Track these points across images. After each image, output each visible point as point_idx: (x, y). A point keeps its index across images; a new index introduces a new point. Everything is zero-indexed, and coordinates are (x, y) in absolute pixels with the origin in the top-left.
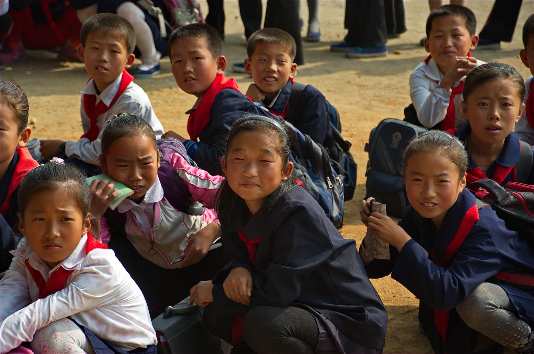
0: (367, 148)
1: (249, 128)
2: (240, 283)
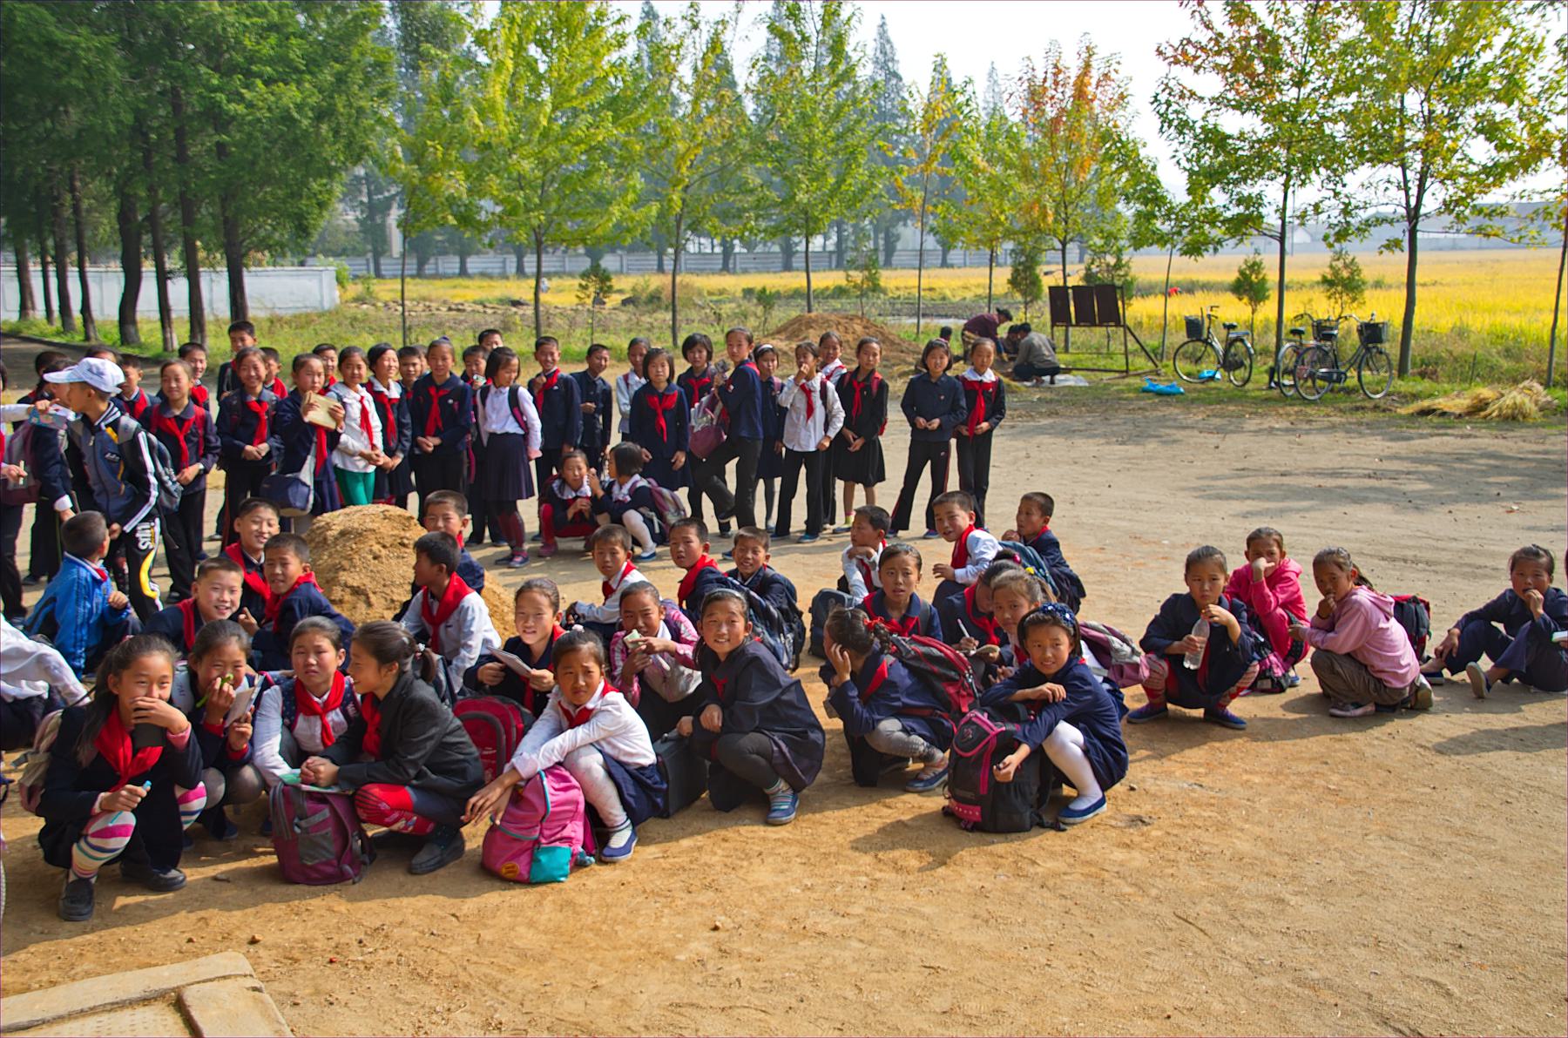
0: (810, 610)
1: (718, 599)
2: (713, 716)
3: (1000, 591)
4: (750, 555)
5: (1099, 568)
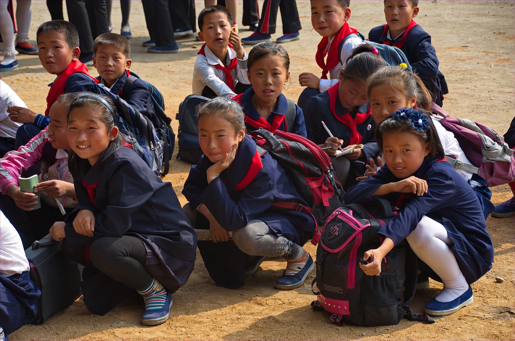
0: (178, 117)
2: (86, 221)
3: (378, 88)
4: (111, 62)
5: (462, 66)
